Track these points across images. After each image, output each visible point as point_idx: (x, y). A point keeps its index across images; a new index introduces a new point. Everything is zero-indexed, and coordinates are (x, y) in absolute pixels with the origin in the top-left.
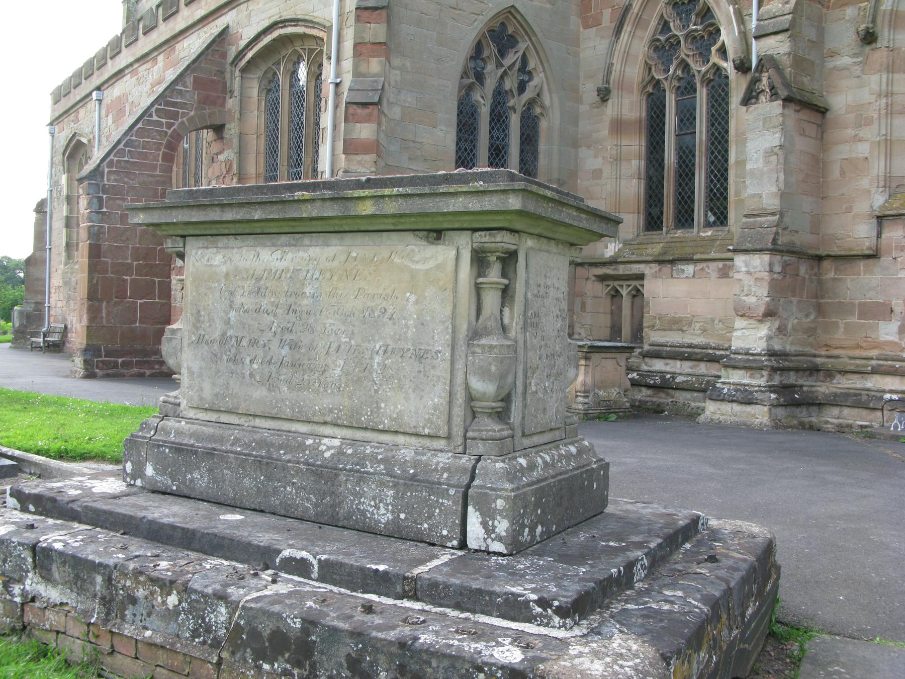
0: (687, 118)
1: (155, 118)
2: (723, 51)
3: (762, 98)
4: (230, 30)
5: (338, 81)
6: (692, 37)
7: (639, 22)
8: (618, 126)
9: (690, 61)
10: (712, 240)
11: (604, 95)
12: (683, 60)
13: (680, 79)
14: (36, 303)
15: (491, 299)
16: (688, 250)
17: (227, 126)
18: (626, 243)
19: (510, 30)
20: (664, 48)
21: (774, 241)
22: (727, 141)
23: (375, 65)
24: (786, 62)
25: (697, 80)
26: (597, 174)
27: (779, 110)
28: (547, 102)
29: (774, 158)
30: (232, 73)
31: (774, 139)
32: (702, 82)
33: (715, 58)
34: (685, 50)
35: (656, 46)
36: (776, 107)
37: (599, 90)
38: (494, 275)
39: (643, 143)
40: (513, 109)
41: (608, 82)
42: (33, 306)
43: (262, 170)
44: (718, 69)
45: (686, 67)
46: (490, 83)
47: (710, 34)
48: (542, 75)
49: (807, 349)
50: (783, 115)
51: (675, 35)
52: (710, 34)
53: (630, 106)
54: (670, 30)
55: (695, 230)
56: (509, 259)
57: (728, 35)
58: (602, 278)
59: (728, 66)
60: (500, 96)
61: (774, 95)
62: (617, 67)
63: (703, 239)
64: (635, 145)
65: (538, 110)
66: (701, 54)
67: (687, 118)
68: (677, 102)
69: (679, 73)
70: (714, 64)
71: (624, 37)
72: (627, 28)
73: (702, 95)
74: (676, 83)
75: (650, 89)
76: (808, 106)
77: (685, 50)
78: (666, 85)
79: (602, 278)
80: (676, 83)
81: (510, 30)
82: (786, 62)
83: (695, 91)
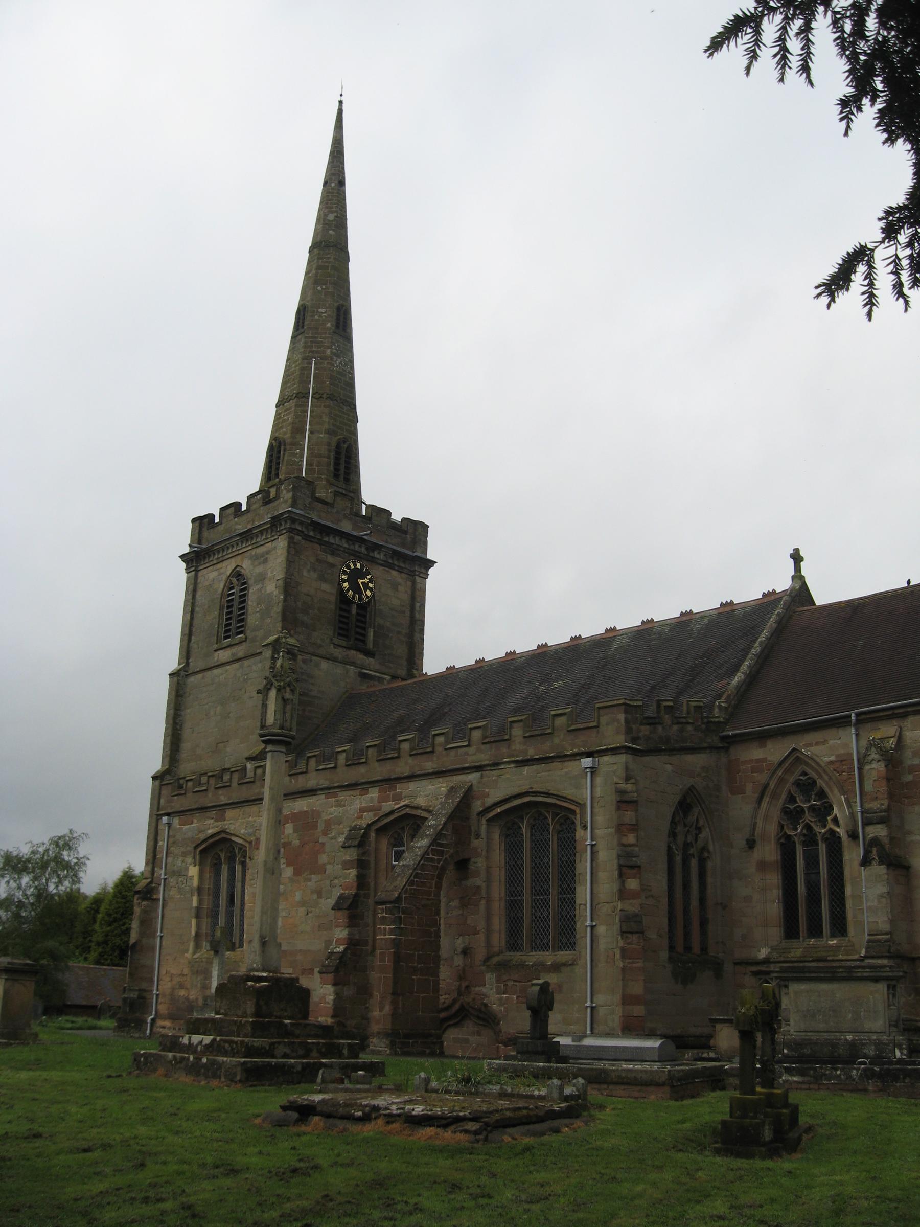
0: (812, 862)
1: (431, 856)
2: (836, 821)
3: (874, 863)
4: (475, 788)
5: (594, 842)
6: (812, 808)
7: (775, 796)
8: (763, 866)
9: (812, 825)
10: (838, 947)
11: (751, 844)
12: (807, 824)
13: (805, 835)
14: (140, 990)
15: (891, 996)
16: (824, 954)
17: (473, 860)
18: (773, 949)
19: (689, 801)
20: (792, 815)
21: (889, 952)
22: (842, 880)
23: (631, 839)
24: (886, 841)
25: (819, 838)
26: (748, 899)
27: (885, 871)
28: (711, 848)
29: (884, 900)
30: (479, 821)
31: (882, 889)
32: (822, 840)
33: (830, 825)
34: (808, 817)
35: (785, 811)
36: (882, 870)
37: (748, 841)
38: (891, 991)
39: (780, 877)
40: (693, 856)
41: (753, 835)
42: (137, 993)
43: (503, 895)
44: (832, 832)
45: (808, 827)
46: (680, 839)
47: (825, 807)
48: (708, 830)
49: (912, 1017)
50: (887, 874)
51: (800, 806)
52: (825, 807)
53: (769, 852)
54: (797, 802)
55: (825, 939)
56: (894, 987)
57: (839, 810)
58: (755, 974)
59: (841, 831)
60: (687, 845)
61: (881, 862)
62: (760, 824)
63: (832, 946)
64: (774, 879)
65: (706, 854)
66: (820, 821)
67: (812, 862)
68: (804, 851)
69: (804, 831)
70: (830, 829)
71: (764, 805)
72: (766, 799)
73: (822, 848)
74: (802, 839)
75: (783, 840)
76: (897, 864)
77: (808, 817)
78: (796, 839)
79: (755, 974)
80: (802, 839)
81: (689, 801)
82: (886, 841)
83: (817, 845)
